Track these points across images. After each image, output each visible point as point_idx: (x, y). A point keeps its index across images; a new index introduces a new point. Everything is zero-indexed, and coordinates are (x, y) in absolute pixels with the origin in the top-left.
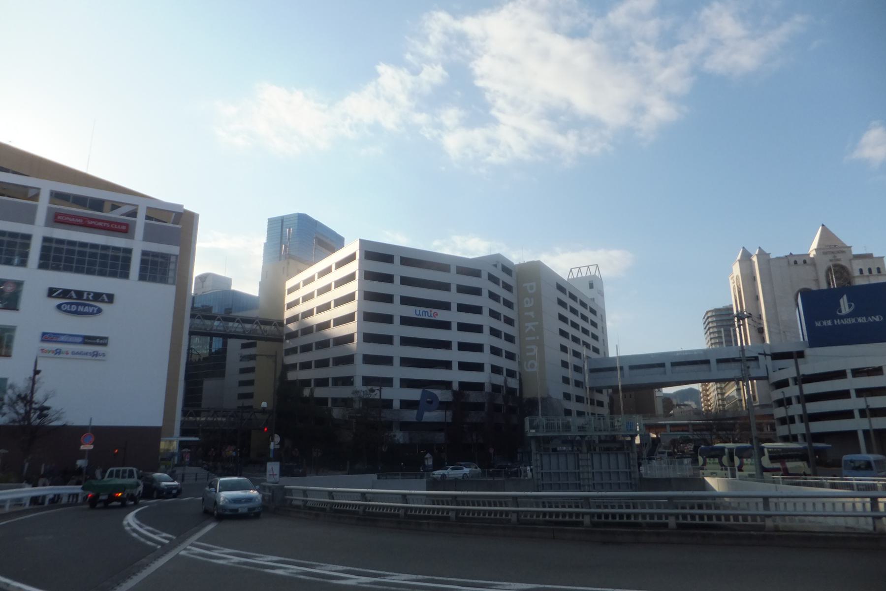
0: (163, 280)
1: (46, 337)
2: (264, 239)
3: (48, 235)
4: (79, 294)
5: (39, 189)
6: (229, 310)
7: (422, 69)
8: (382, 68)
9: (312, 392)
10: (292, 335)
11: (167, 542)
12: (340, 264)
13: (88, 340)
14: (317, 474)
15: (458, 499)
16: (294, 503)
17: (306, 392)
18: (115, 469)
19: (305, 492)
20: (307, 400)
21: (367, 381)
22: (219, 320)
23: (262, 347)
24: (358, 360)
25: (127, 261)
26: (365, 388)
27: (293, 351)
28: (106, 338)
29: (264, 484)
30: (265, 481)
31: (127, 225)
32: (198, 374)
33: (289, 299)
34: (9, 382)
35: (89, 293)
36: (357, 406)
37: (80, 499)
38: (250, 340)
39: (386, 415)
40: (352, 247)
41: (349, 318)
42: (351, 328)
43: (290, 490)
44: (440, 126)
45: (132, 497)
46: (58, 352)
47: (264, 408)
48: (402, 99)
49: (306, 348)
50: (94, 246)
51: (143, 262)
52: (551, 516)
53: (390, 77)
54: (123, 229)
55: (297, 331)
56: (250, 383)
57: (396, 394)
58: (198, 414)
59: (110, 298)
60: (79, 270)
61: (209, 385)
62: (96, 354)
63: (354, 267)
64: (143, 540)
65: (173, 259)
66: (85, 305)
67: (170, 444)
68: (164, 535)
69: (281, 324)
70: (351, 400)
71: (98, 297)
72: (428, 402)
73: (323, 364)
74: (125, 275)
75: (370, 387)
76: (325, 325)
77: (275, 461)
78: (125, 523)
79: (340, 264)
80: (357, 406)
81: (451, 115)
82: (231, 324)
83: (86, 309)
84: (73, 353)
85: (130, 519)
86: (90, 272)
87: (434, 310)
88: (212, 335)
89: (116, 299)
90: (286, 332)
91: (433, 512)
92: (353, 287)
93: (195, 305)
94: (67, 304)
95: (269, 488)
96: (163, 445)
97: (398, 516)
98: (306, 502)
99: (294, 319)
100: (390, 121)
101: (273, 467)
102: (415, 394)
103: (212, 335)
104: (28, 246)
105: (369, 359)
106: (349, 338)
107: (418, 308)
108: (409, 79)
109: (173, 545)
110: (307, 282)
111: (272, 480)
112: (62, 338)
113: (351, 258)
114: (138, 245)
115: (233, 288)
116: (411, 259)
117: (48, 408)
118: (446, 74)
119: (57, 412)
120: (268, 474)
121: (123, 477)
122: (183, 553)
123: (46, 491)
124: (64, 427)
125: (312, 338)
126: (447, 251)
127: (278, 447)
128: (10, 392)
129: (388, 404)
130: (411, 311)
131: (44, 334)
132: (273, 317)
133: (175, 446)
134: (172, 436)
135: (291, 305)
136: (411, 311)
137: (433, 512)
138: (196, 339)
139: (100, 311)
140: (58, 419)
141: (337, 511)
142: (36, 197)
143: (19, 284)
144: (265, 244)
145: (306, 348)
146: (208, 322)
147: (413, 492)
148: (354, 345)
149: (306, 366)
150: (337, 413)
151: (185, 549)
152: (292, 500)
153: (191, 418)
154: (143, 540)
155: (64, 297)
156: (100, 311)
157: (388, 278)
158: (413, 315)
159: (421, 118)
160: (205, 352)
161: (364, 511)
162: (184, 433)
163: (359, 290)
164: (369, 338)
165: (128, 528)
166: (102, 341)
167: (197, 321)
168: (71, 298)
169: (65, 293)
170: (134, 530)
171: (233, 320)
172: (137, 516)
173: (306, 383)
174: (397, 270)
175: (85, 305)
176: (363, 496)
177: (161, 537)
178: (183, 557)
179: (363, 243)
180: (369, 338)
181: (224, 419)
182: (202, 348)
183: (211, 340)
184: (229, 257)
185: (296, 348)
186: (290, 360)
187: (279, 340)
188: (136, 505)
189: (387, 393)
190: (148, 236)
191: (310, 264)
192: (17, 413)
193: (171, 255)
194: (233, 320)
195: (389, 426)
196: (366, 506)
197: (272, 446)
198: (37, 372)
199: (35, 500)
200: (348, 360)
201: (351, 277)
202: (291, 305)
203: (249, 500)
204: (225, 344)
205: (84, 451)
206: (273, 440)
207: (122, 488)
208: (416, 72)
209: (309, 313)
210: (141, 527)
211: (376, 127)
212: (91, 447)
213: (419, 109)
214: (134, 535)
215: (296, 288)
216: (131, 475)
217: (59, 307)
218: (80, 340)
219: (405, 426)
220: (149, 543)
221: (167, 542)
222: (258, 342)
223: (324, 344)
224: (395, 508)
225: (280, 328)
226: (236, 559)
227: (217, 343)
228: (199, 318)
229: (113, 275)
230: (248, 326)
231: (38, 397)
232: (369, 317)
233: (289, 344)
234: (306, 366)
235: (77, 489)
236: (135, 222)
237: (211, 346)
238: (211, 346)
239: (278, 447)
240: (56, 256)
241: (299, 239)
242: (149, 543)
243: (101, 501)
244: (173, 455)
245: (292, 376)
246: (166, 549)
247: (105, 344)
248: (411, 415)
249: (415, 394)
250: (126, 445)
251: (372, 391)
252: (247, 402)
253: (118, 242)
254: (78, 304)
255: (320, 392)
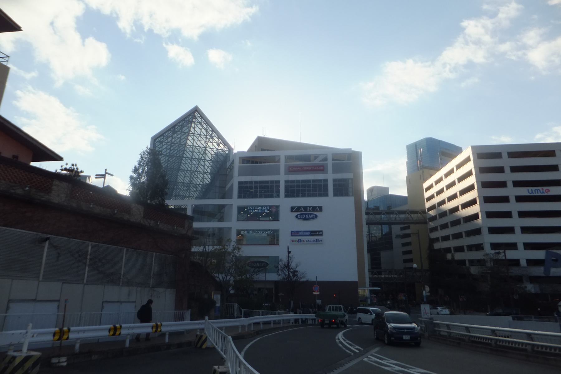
0: (346, 194)
1: (294, 233)
2: (406, 160)
3: (287, 179)
4: (305, 208)
5: (280, 156)
6: (389, 207)
7: (499, 11)
8: (465, 23)
9: (453, 256)
10: (433, 218)
11: (358, 351)
12: (459, 166)
13: (313, 233)
14: (465, 314)
15: (533, 336)
16: (442, 333)
17: (449, 256)
18: (331, 306)
19: (448, 326)
20: (453, 261)
21: (494, 246)
22: (384, 214)
23: (413, 228)
24: (485, 231)
25: (326, 186)
26: (493, 252)
27: (435, 229)
28: (322, 231)
29: (420, 319)
30: (421, 317)
31: (323, 166)
32: (376, 250)
33: (427, 195)
34: (280, 258)
35: (310, 207)
36: (489, 264)
37: (316, 322)
38: (406, 225)
39: (515, 271)
40: (467, 152)
41: (472, 202)
42: (475, 209)
43: (438, 324)
44: (525, 47)
45: (342, 323)
46: (299, 241)
47: (415, 268)
48: (487, 38)
49: (444, 226)
50: (309, 181)
51: (334, 186)
52: (546, 349)
53: (473, 27)
54: (321, 169)
55: (436, 216)
56: (410, 252)
57: (522, 255)
58: (380, 273)
59: (320, 209)
60: (314, 195)
61: (384, 255)
62: (317, 241)
63: (470, 166)
64: (344, 349)
65: (350, 181)
66: (309, 214)
67: (365, 291)
68: (357, 347)
69: (424, 212)
70: (484, 260)
71: (314, 209)
72: (553, 260)
73: (458, 236)
74: (326, 195)
75: (497, 251)
76: (456, 209)
77: (428, 303)
78: (337, 337)
79: (459, 166)
80: (489, 264)
81: (531, 36)
82: (392, 216)
83: (310, 216)
84: (306, 241)
85: (340, 336)
86: (309, 196)
87: (545, 188)
88: (381, 224)
89: (323, 209)
90: (428, 217)
91: (542, 349)
92: (472, 180)
93: (369, 207)
94: (300, 214)
95: (424, 321)
96: (361, 292)
97: (525, 350)
98: (451, 333)
99: (432, 208)
100: (479, 57)
101: (425, 308)
102: (540, 255)
103: (381, 224)
104: (279, 186)
105: (493, 230)
106: (475, 216)
107: (530, 189)
108: (489, 23)
109: (361, 354)
110: (437, 182)
111: (426, 316)
112: (300, 233)
113: (467, 160)
114: (330, 176)
115: (390, 193)
116: (518, 152)
117: (297, 272)
118: (520, 6)
119: (303, 273)
120: (422, 312)
121: (337, 310)
122: (365, 359)
123: (299, 316)
124: (307, 281)
125: (448, 219)
126: (550, 140)
127: (429, 294)
128: (280, 263)
129: (516, 263)
130: (523, 191)
131: (292, 232)
132: (418, 208)
133: (367, 293)
134: (365, 287)
135: (429, 199)
136: (523, 191)
137: (522, 346)
138: (374, 227)
139: (316, 216)
140: (304, 277)
141: (473, 342)
142: (279, 161)
143: (278, 207)
144: (407, 162)
145: (444, 226)
146: (378, 216)
147: (472, 326)
148: (480, 221)
149: (446, 238)
150: (474, 270)
151: (367, 357)
152: (440, 331)
153: (376, 276)
154: (344, 349)
155: (298, 211)
156: (316, 216)
157: (500, 170)
158: (526, 194)
159: (506, 47)
160: (379, 235)
161: (496, 343)
162: (373, 284)
163: (477, 181)
164: (490, 215)
165: (337, 341)
166: (319, 233)
167: (371, 216)
168: (302, 211)
169: (298, 209)
170: (341, 343)
171: (392, 213)
172: (344, 335)
173: (448, 250)
174: (506, 162)
175: (309, 214)
176: (493, 332)
177: (355, 348)
178: (365, 362)
179: (474, 148)
180: (490, 215)
181: (396, 276)
182: (377, 232)
183: (382, 227)
184: (385, 173)
185: (437, 227)
186: (434, 235)
187: (425, 223)
188: (345, 327)
189: (511, 254)
190: (335, 171)
191: (438, 170)
192: (285, 274)
193: (349, 179)
194: (392, 213)
195: (520, 279)
196: (497, 340)
197: (424, 293)
198: (289, 252)
199: (296, 321)
200: (477, 232)
201: (469, 174)
202: (429, 199)
203: (414, 328)
204: (390, 229)
205: (315, 295)
206: (424, 289)
207: (336, 317)
208: (493, 15)
209: (443, 202)
210: (345, 341)
211: (470, 65)
212: (319, 293)
213: (502, 41)
214: (340, 345)
215: (431, 187)
216: (340, 310)
217: (297, 216)
218: (309, 233)
219: (533, 279)
220: (347, 351)
221: (358, 351)
222: (411, 226)
223: (457, 222)
224: (523, 344)
225: (424, 215)
226: (397, 368)
227: (386, 229)
228: (372, 214)
229: (320, 195)
230: (402, 216)
231: (293, 265)
232: (487, 200)
233: (432, 224)
234: (446, 238)
235: (313, 316)
236: (327, 164)
237: (382, 230)
238: (382, 230)
239: (429, 294)
240: (293, 190)
241: (429, 155)
242: (347, 351)
243: (327, 324)
244: (367, 298)
245: (437, 246)
246: (356, 356)
247: (321, 235)
248: (539, 271)
249: (540, 255)
250: (340, 294)
251: (499, 253)
252: (408, 265)
253: (320, 176)
254: (305, 214)
255: (459, 256)
